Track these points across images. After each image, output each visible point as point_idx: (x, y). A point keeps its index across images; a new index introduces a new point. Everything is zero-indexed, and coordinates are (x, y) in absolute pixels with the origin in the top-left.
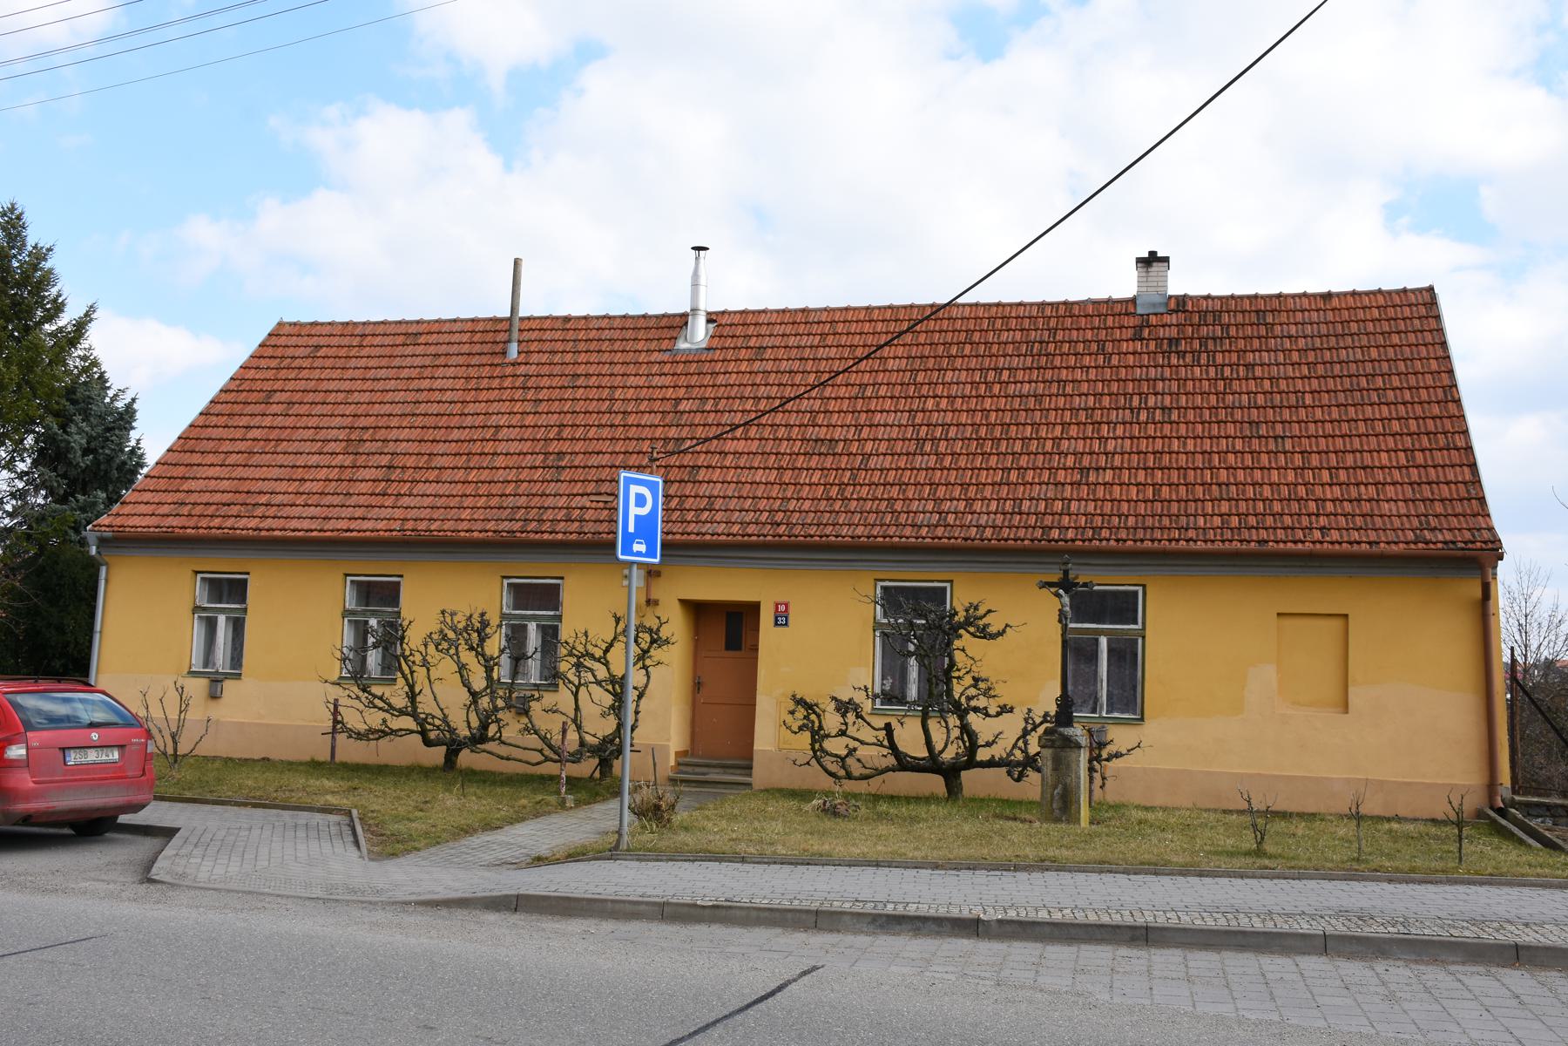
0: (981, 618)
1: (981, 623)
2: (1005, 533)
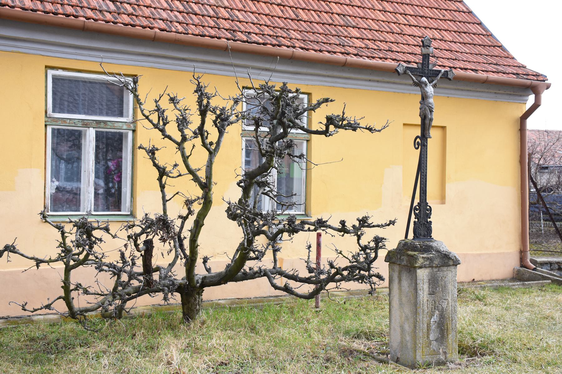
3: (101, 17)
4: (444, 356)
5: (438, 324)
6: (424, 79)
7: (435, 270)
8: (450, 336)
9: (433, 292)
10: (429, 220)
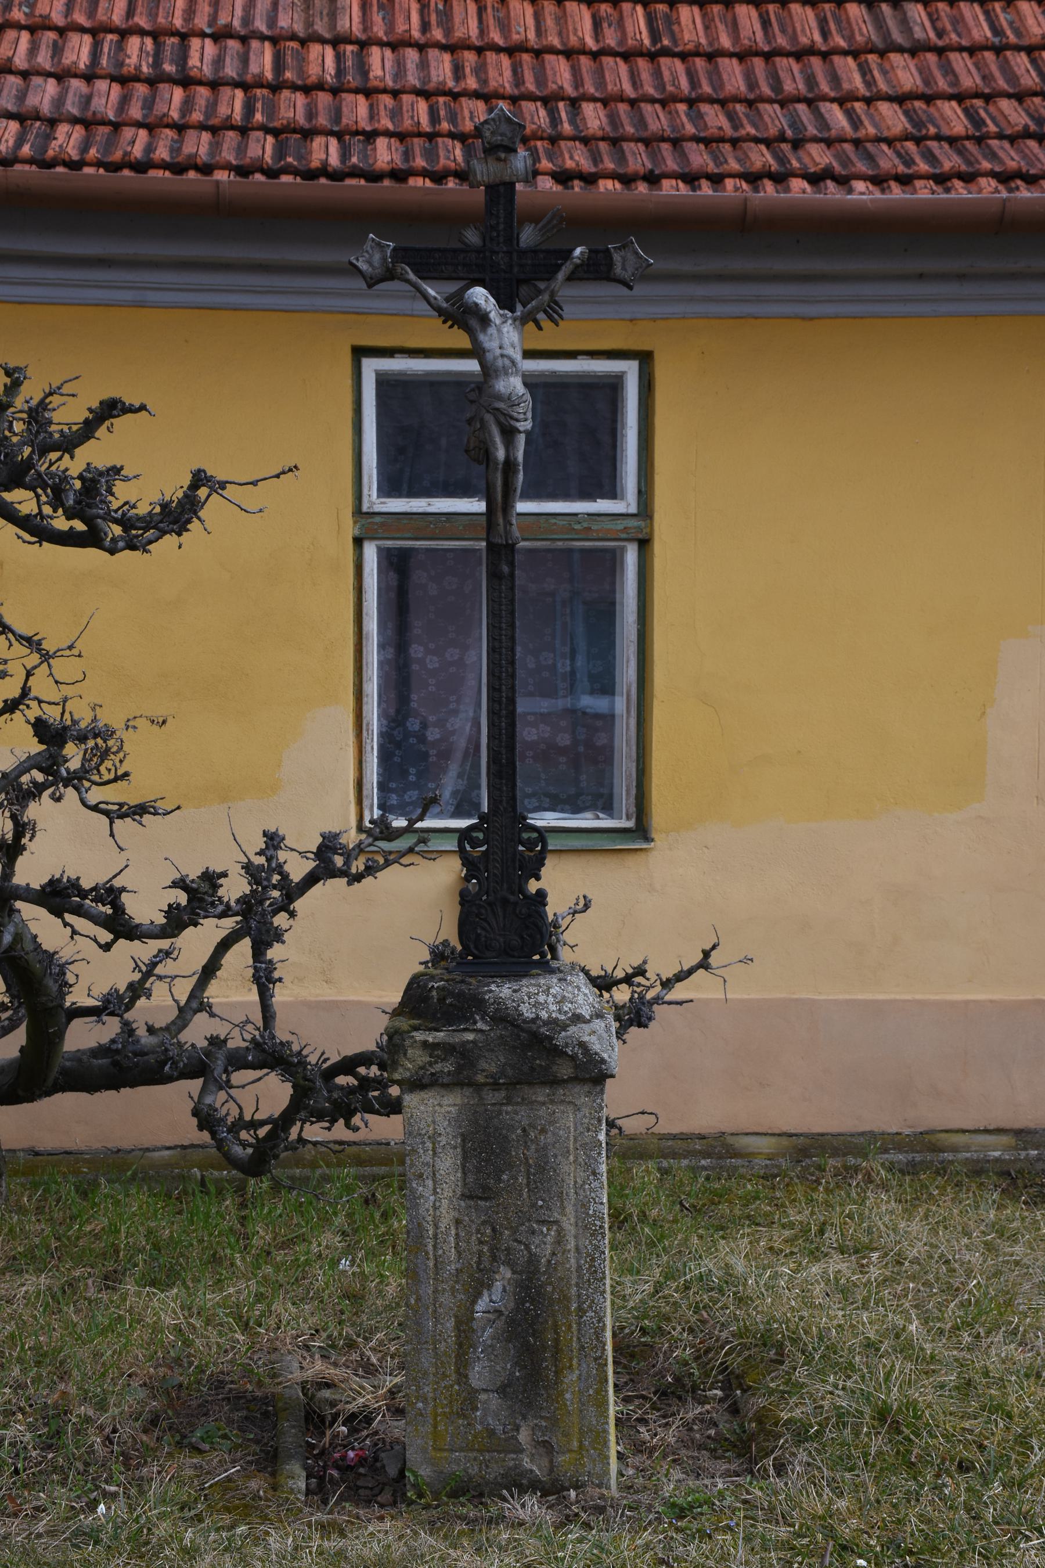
0: (69, 444)
1: (74, 465)
2: (136, 143)
3: (861, 167)
4: (545, 1462)
5: (511, 1322)
6: (479, 295)
7: (491, 1097)
8: (571, 1377)
9: (485, 1188)
10: (533, 886)
